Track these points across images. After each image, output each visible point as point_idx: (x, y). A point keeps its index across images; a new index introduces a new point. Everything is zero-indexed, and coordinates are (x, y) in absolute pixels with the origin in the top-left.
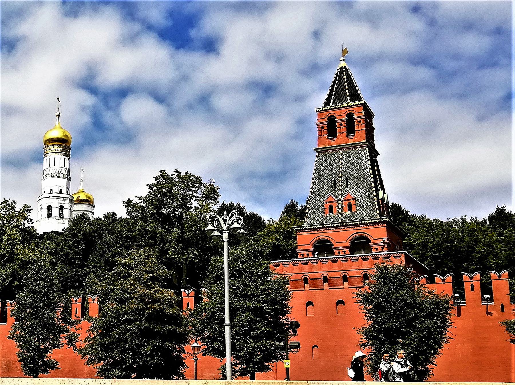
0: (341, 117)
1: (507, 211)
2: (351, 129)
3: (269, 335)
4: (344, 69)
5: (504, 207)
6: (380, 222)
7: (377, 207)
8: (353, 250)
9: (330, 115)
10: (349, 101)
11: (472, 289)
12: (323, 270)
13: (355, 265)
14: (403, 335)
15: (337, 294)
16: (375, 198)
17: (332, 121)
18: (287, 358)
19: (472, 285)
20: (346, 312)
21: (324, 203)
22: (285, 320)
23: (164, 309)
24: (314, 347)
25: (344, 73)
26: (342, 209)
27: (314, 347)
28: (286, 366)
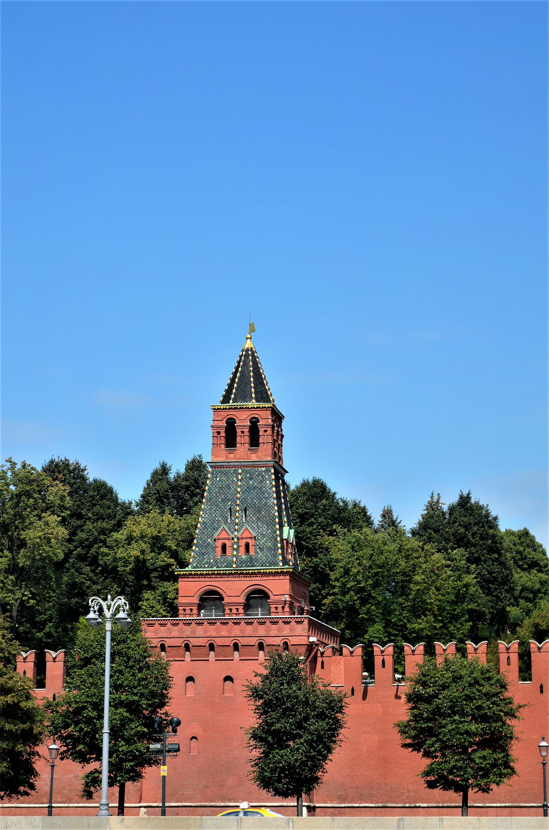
0: (243, 421)
1: (473, 501)
2: (254, 442)
3: (141, 736)
4: (250, 352)
5: (469, 494)
6: (282, 573)
7: (280, 551)
8: (247, 607)
9: (230, 417)
10: (254, 401)
11: (383, 666)
12: (209, 634)
13: (249, 630)
14: (295, 737)
15: (225, 669)
16: (279, 539)
17: (231, 425)
18: (164, 765)
19: (383, 660)
20: (234, 692)
21: (215, 540)
22: (163, 714)
23: (19, 702)
24: (192, 739)
25: (250, 357)
26: (237, 550)
27: (192, 739)
28: (163, 774)
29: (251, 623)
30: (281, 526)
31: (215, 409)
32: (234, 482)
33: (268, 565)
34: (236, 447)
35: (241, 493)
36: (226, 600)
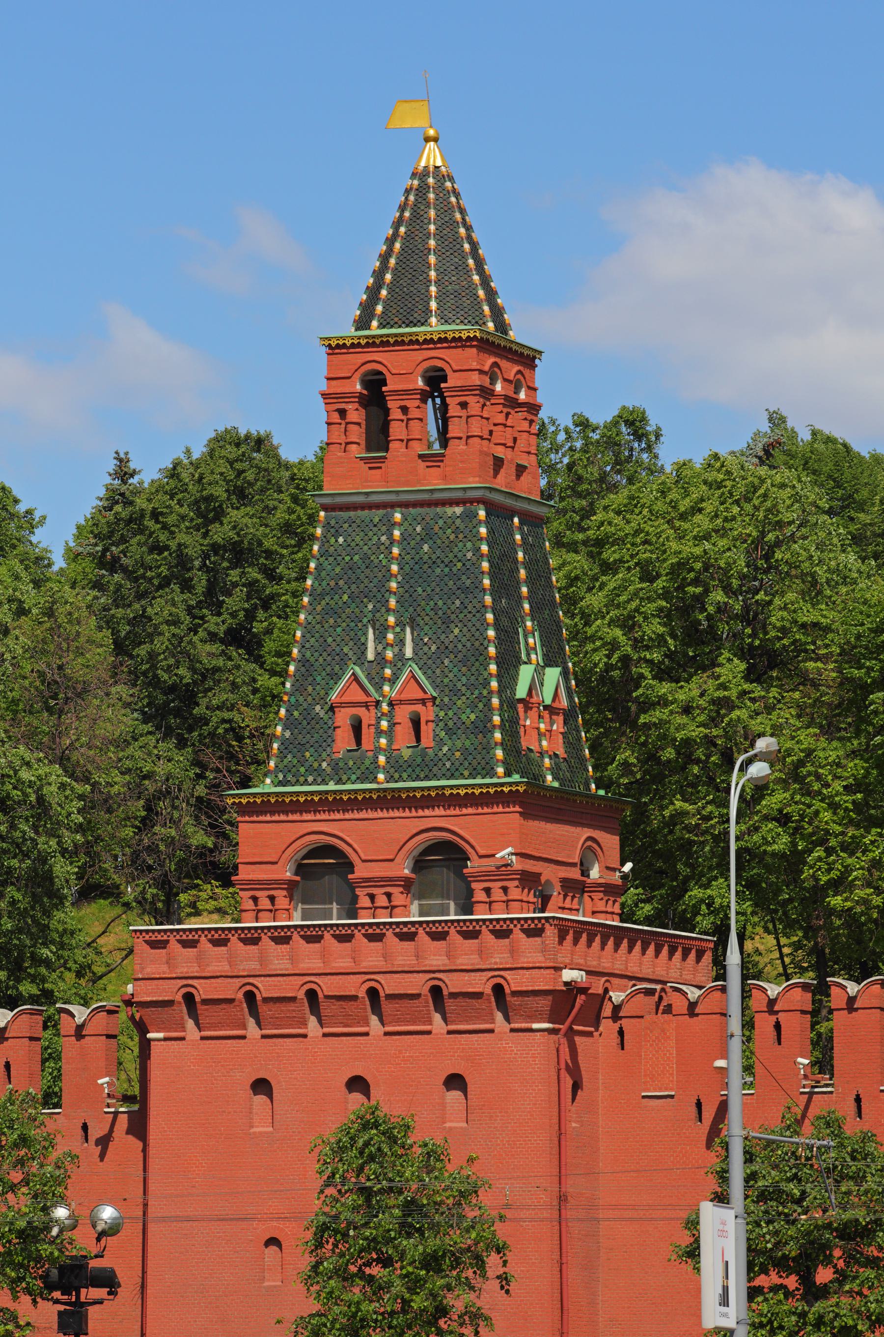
0: (405, 373)
4: (431, 180)
10: (433, 320)
26: (390, 734)
29: (318, 939)
30: (509, 662)
31: (330, 346)
32: (382, 547)
33: (466, 773)
34: (387, 450)
35: (400, 578)
36: (361, 871)
